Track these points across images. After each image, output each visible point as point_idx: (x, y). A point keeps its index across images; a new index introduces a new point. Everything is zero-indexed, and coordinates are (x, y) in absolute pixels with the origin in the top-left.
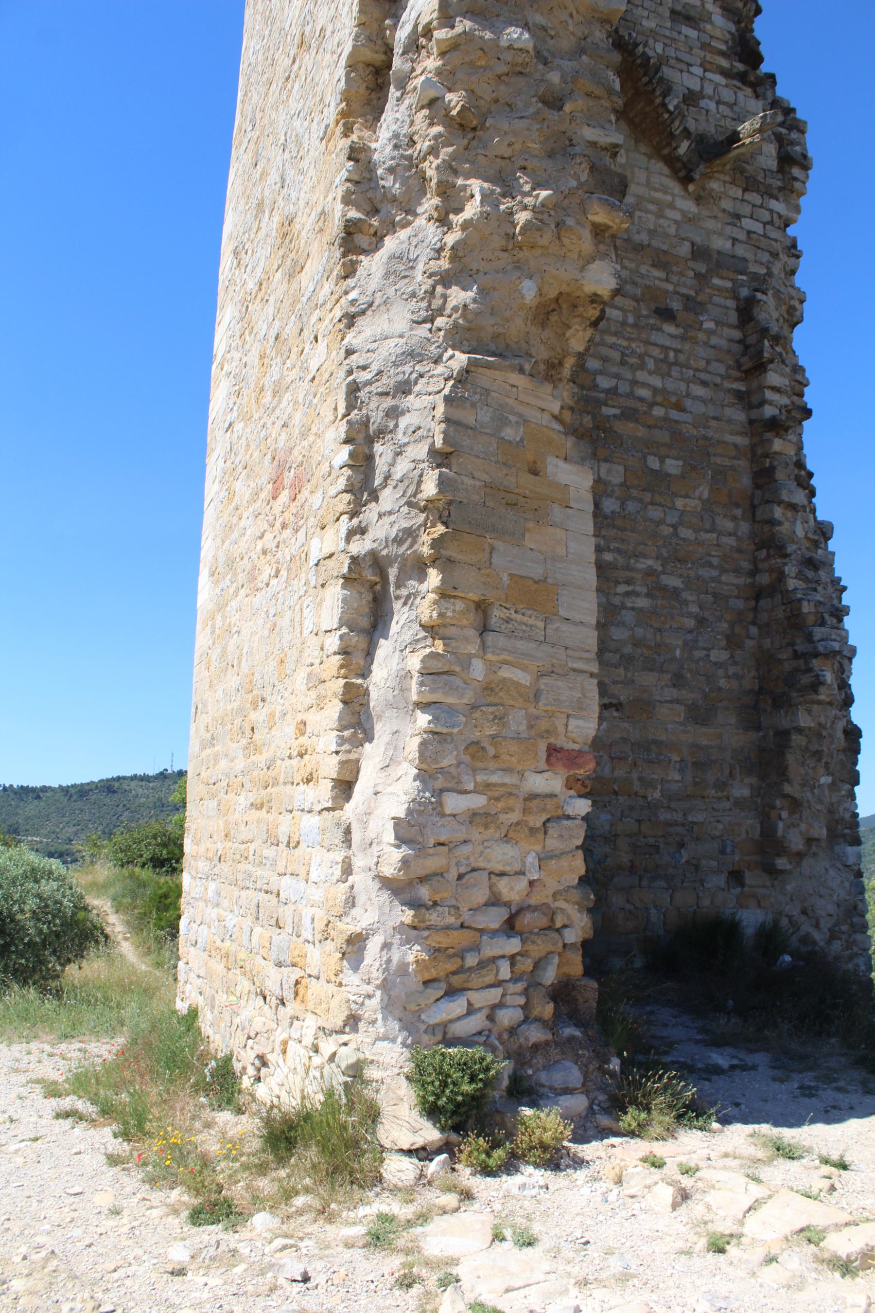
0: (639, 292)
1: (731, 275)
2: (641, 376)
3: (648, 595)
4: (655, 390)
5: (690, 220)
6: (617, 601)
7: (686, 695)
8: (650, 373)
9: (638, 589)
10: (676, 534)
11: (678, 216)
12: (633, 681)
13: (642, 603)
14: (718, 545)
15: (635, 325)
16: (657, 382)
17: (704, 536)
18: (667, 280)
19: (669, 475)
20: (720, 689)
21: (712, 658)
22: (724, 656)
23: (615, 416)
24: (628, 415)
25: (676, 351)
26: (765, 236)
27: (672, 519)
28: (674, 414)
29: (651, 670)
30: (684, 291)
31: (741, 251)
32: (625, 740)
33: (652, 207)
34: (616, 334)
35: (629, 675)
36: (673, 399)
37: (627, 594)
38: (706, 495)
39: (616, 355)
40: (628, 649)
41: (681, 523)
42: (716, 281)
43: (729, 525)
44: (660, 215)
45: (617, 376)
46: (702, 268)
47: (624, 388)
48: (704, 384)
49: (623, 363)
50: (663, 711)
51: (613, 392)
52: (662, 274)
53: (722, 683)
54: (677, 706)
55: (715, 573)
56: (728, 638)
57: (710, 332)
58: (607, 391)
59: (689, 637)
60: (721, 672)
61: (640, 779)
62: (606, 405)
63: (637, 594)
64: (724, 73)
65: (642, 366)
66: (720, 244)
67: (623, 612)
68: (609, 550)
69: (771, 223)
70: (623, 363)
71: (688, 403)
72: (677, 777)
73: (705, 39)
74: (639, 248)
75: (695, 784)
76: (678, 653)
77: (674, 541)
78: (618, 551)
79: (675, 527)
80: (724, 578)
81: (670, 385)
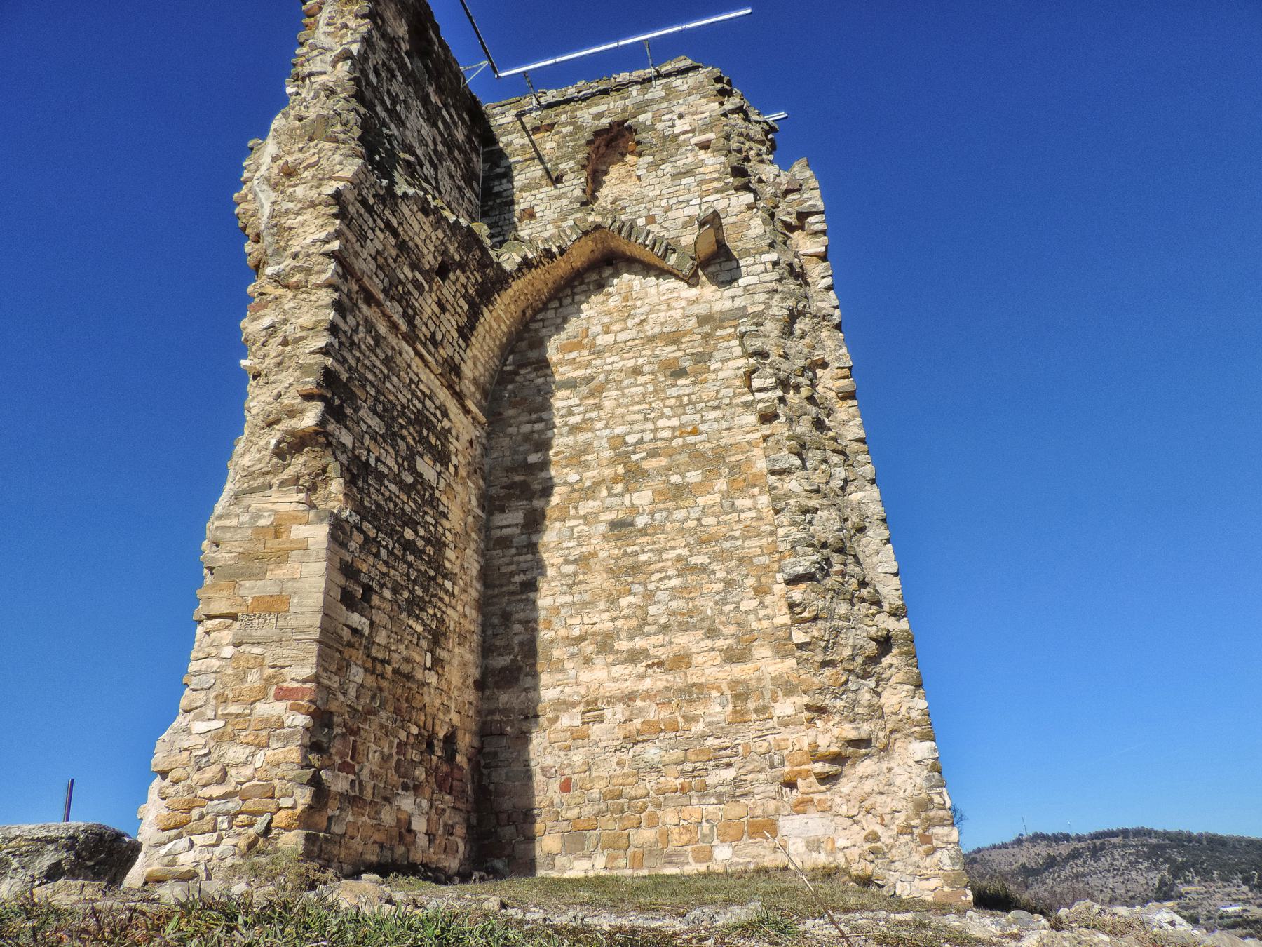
0: (656, 367)
1: (732, 323)
2: (661, 423)
3: (679, 576)
4: (673, 428)
5: (696, 301)
6: (651, 587)
7: (720, 643)
8: (669, 418)
9: (670, 573)
10: (700, 524)
11: (684, 303)
12: (671, 643)
13: (676, 582)
14: (739, 521)
15: (655, 391)
16: (675, 422)
17: (724, 518)
18: (679, 350)
19: (690, 484)
20: (752, 631)
21: (742, 608)
22: (754, 603)
23: (642, 459)
24: (653, 454)
25: (688, 395)
26: (761, 282)
27: (695, 513)
28: (691, 439)
29: (686, 630)
30: (695, 351)
31: (739, 302)
32: (667, 689)
33: (664, 307)
34: (639, 403)
35: (667, 639)
36: (690, 429)
37: (661, 579)
38: (724, 487)
39: (640, 417)
40: (663, 620)
41: (704, 514)
42: (719, 333)
43: (748, 503)
44: (669, 308)
45: (643, 431)
46: (707, 329)
47: (648, 436)
48: (715, 408)
49: (646, 419)
50: (697, 660)
51: (641, 441)
52: (674, 348)
53: (755, 625)
54: (712, 653)
55: (738, 543)
56: (755, 589)
57: (716, 371)
58: (635, 444)
59: (718, 597)
60: (751, 617)
61: (683, 717)
62: (635, 453)
63: (670, 578)
64: (717, 191)
65: (662, 416)
66: (717, 307)
67: (659, 593)
68: (643, 552)
69: (766, 271)
70: (646, 419)
71: (703, 427)
72: (719, 709)
73: (698, 178)
74: (651, 339)
75: (735, 712)
76: (709, 612)
77: (699, 529)
78: (652, 550)
79: (699, 520)
80: (747, 544)
81: (684, 419)
